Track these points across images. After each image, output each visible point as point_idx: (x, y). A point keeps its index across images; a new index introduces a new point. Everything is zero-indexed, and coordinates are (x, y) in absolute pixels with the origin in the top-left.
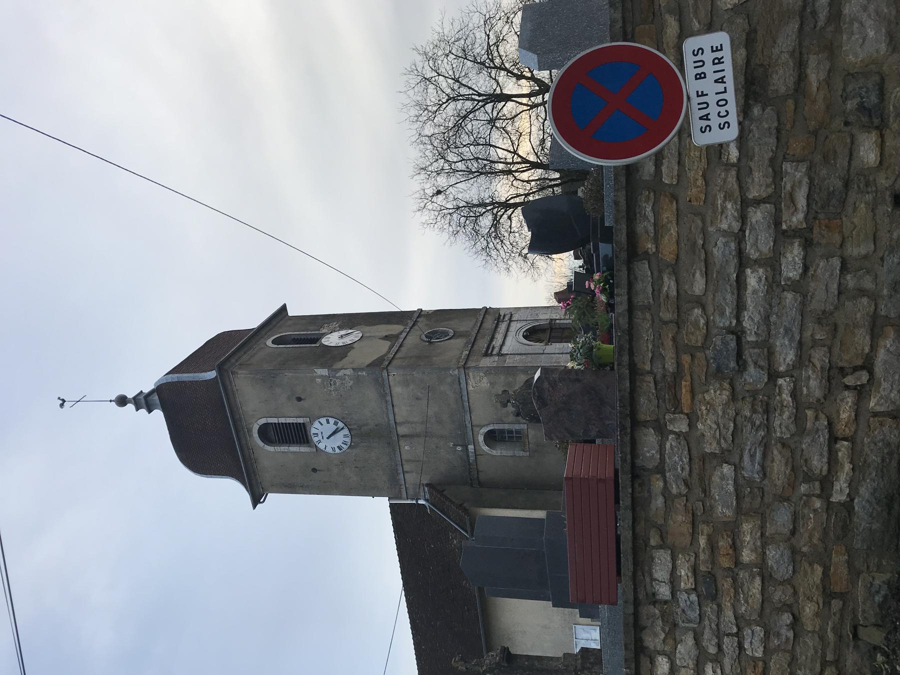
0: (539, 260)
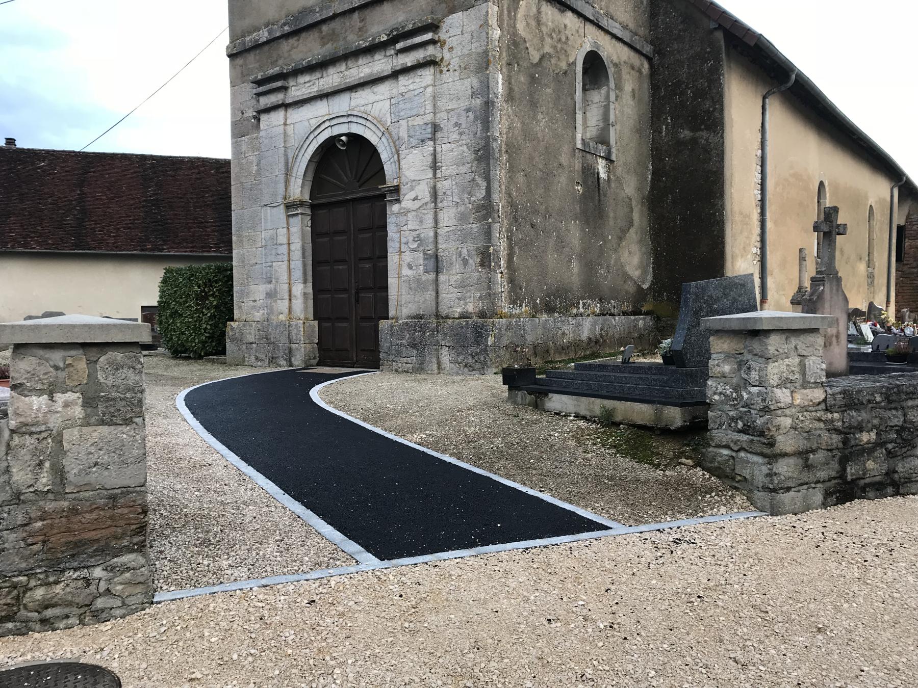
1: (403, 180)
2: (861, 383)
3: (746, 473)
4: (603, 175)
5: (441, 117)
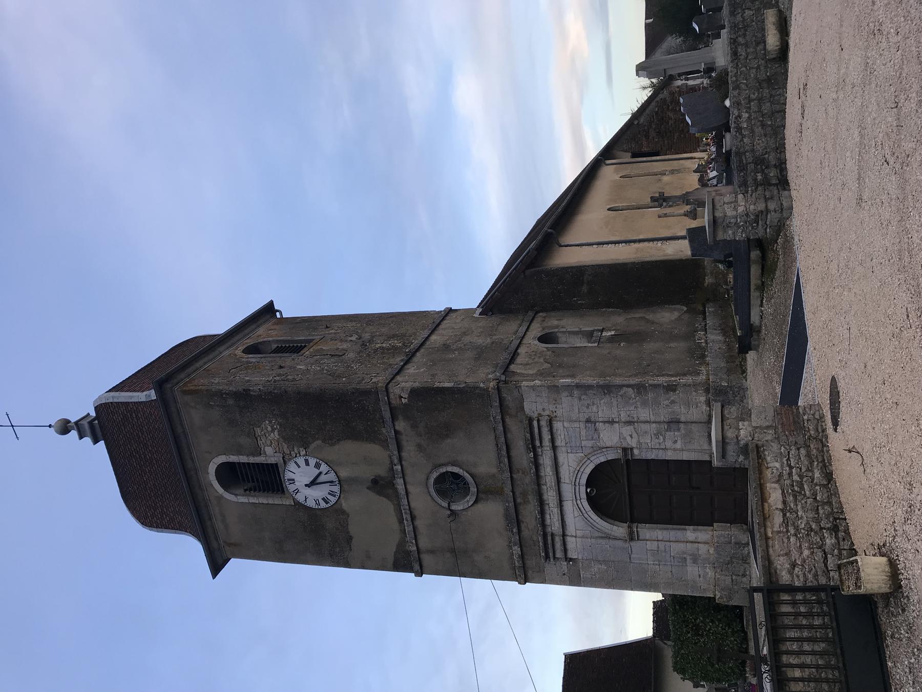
0: (792, 185)
1: (618, 445)
2: (736, 180)
3: (776, 221)
4: (613, 333)
5: (583, 417)
